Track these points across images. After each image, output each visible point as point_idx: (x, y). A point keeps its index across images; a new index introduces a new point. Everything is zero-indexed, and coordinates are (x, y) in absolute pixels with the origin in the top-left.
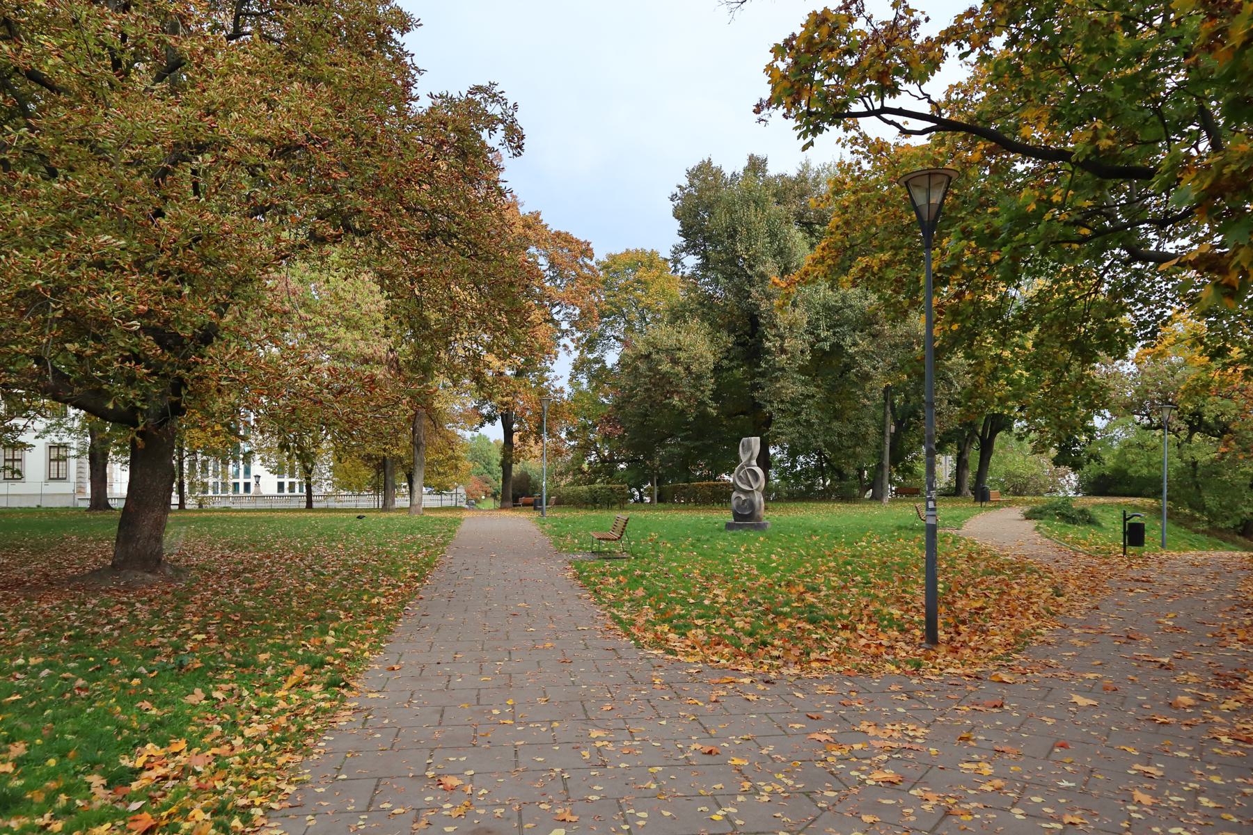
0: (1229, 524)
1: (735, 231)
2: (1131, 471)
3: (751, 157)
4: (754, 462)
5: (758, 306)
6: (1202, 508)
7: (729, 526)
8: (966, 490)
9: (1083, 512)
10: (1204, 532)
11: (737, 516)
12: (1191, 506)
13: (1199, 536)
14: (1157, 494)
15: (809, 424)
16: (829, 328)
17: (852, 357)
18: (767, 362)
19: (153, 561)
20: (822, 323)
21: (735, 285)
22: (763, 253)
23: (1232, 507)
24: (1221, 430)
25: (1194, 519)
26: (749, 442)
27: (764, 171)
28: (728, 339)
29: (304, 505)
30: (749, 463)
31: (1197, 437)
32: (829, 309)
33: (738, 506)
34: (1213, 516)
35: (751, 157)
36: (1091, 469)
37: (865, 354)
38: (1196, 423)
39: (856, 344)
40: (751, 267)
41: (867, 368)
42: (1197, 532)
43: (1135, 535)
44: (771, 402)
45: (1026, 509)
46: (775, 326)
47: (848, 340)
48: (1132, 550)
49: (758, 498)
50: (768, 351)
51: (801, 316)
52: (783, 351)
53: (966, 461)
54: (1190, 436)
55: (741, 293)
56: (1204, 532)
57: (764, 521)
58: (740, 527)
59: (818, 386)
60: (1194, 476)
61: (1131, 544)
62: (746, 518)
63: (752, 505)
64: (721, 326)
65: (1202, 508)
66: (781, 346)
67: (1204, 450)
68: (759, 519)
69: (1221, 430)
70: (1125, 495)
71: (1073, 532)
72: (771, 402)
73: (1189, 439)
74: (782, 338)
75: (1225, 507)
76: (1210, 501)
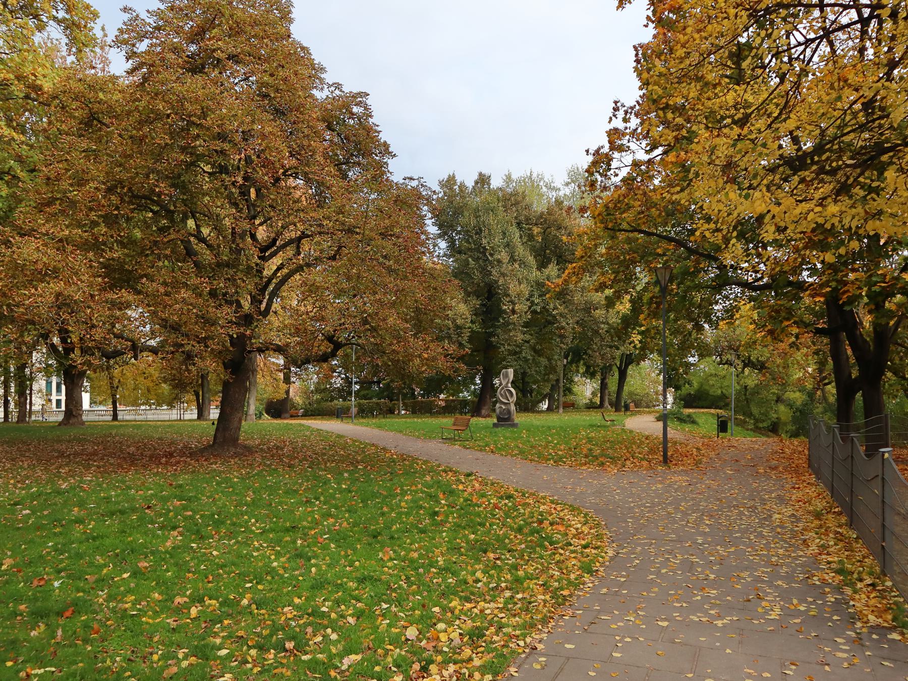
0: (765, 425)
1: (481, 230)
2: (711, 392)
3: (480, 174)
4: (510, 385)
5: (496, 282)
6: (750, 415)
7: (495, 425)
8: (607, 404)
9: (689, 416)
10: (751, 430)
11: (499, 419)
12: (744, 414)
13: (749, 432)
14: (726, 406)
15: (526, 360)
16: (540, 296)
17: (554, 317)
18: (504, 319)
19: (234, 441)
20: (536, 294)
21: (480, 266)
22: (499, 246)
23: (766, 414)
24: (761, 366)
25: (745, 422)
26: (507, 373)
27: (489, 184)
28: (476, 302)
29: (110, 418)
30: (507, 386)
31: (747, 371)
32: (539, 285)
33: (501, 413)
34: (757, 421)
35: (480, 174)
36: (686, 389)
37: (561, 315)
38: (748, 363)
39: (557, 308)
40: (491, 255)
41: (564, 324)
42: (747, 430)
43: (723, 427)
44: (503, 345)
45: (658, 415)
46: (509, 295)
47: (552, 306)
48: (721, 435)
49: (513, 407)
50: (505, 312)
51: (525, 289)
52: (514, 312)
53: (606, 384)
54: (743, 369)
55: (486, 273)
56: (751, 430)
57: (516, 421)
58: (502, 425)
59: (531, 335)
60: (745, 395)
61: (721, 431)
62: (505, 420)
63: (509, 412)
64: (470, 293)
65: (750, 415)
66: (513, 309)
67: (752, 378)
68: (513, 420)
69: (761, 366)
70: (707, 408)
71: (688, 427)
72: (503, 345)
73: (743, 372)
74: (514, 303)
75: (762, 414)
76: (755, 410)
